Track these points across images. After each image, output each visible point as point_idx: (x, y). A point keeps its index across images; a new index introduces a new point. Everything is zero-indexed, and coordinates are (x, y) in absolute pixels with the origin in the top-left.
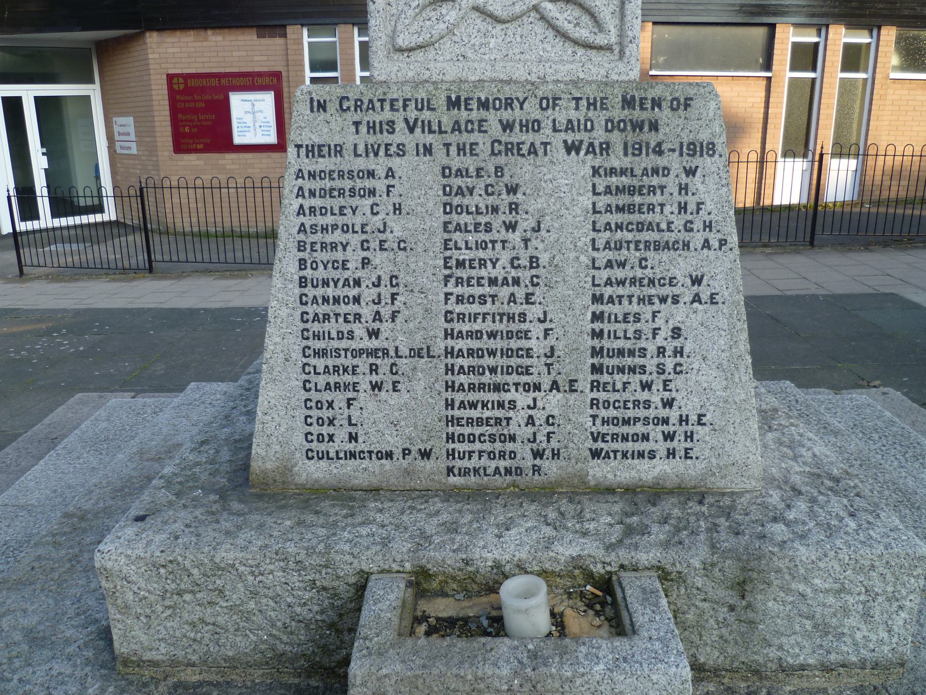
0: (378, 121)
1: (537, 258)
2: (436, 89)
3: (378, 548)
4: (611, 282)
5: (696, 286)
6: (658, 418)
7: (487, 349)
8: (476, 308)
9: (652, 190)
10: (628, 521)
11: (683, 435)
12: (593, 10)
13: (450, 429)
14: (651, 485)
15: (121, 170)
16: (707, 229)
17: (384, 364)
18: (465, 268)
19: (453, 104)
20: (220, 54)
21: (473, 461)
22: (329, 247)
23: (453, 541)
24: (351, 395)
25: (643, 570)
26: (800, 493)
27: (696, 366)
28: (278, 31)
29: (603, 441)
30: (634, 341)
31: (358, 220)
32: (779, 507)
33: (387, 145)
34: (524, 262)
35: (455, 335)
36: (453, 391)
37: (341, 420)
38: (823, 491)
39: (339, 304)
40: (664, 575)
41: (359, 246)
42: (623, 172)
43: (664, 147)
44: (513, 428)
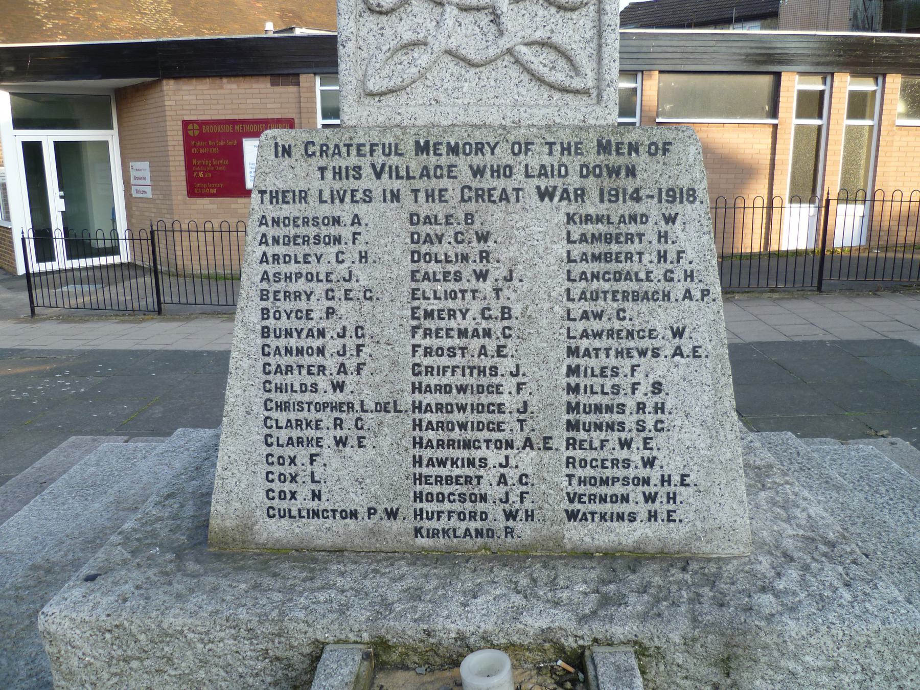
0: (344, 166)
1: (509, 309)
2: (404, 134)
3: (335, 616)
4: (587, 334)
5: (677, 338)
6: (638, 479)
7: (457, 404)
8: (445, 361)
9: (630, 238)
10: (604, 589)
11: (665, 496)
12: (569, 53)
13: (418, 488)
14: (632, 549)
15: (137, 213)
16: (689, 279)
17: (349, 418)
18: (433, 318)
19: (422, 149)
20: (234, 101)
21: (441, 522)
22: (292, 296)
23: (415, 609)
24: (314, 450)
25: (619, 644)
26: (792, 559)
27: (678, 423)
28: (291, 79)
29: (580, 502)
30: (611, 396)
31: (323, 269)
32: (768, 575)
33: (353, 191)
34: (495, 312)
35: (423, 388)
36: (421, 447)
37: (304, 477)
38: (817, 557)
39: (302, 355)
40: (641, 651)
41: (324, 295)
42: (599, 219)
43: (642, 193)
44: (484, 488)
